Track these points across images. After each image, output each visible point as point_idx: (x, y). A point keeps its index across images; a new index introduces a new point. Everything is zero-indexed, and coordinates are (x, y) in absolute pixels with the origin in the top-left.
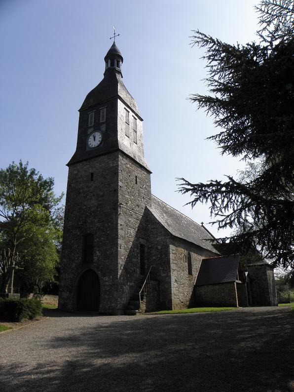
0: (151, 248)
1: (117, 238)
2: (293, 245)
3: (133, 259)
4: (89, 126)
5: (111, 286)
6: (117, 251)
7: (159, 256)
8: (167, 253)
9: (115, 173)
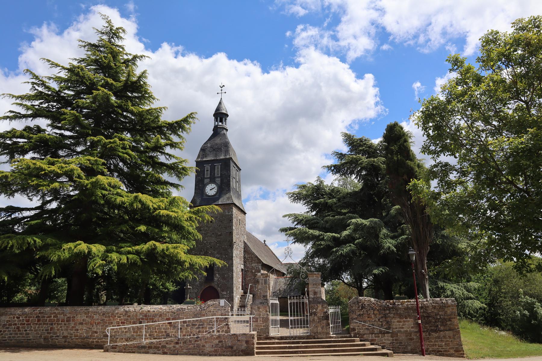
0: (247, 271)
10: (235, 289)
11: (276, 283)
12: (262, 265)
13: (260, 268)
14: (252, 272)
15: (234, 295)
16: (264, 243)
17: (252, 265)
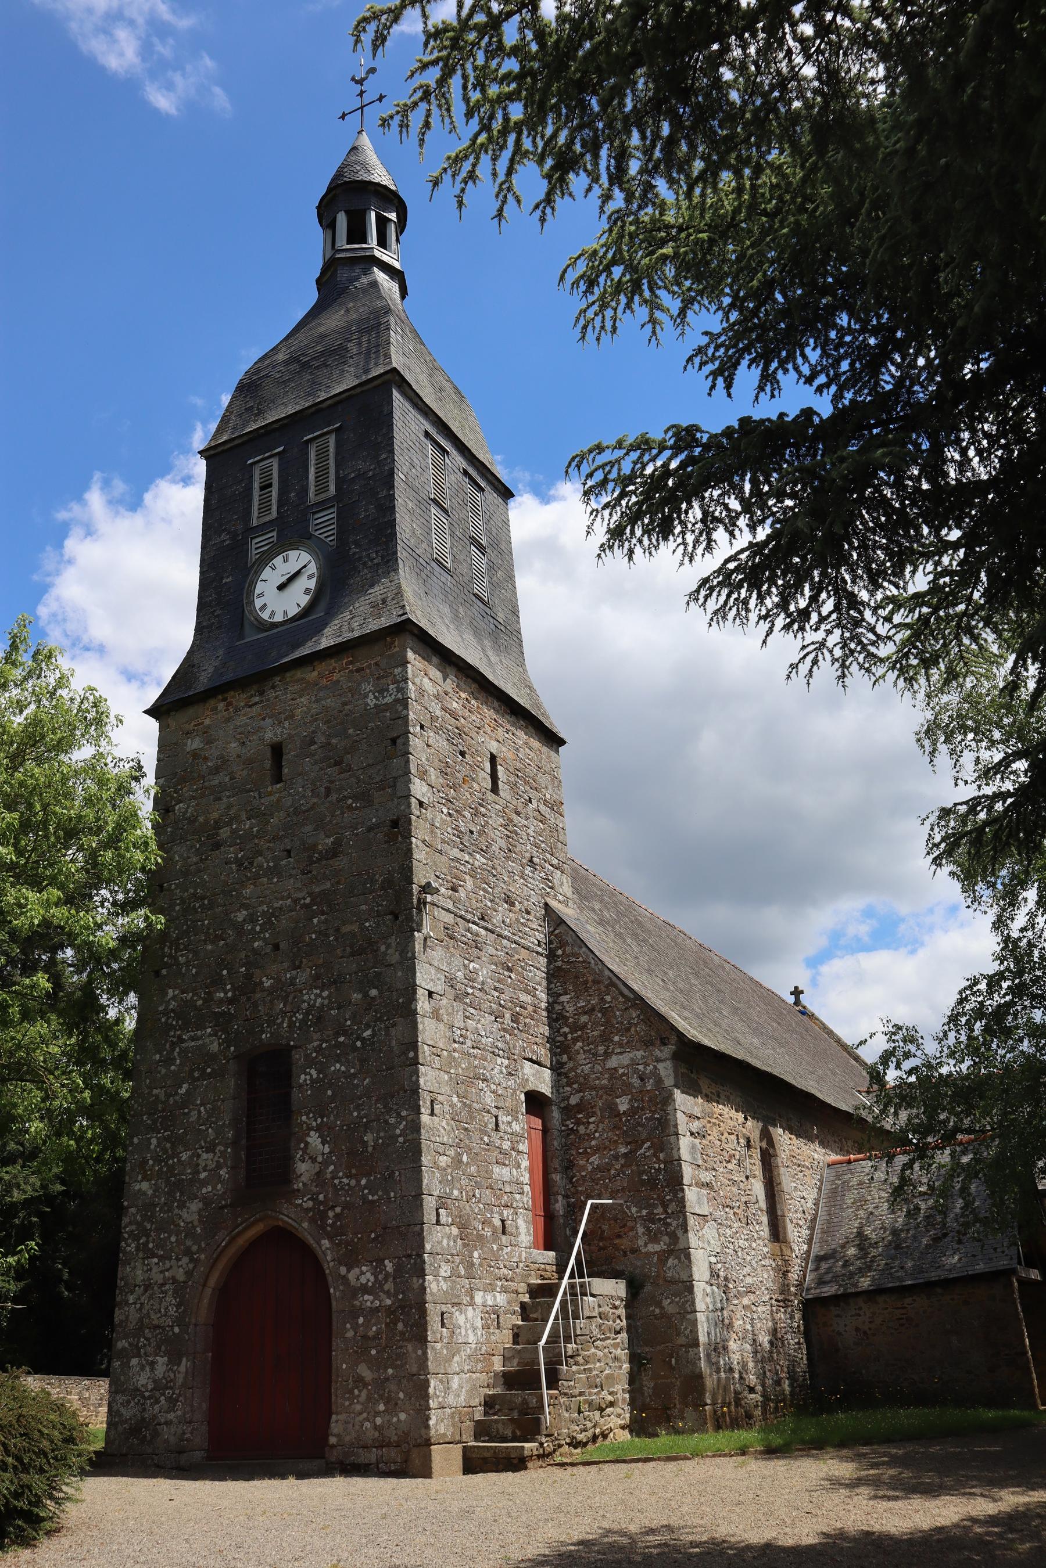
0: (580, 1107)
1: (415, 1062)
3: (497, 1169)
4: (255, 523)
5: (389, 1311)
6: (416, 1127)
7: (623, 1150)
9: (394, 741)
12: (676, 1057)
13: (669, 1081)
14: (612, 1110)
15: (436, 1285)
16: (797, 1002)
17: (613, 1062)
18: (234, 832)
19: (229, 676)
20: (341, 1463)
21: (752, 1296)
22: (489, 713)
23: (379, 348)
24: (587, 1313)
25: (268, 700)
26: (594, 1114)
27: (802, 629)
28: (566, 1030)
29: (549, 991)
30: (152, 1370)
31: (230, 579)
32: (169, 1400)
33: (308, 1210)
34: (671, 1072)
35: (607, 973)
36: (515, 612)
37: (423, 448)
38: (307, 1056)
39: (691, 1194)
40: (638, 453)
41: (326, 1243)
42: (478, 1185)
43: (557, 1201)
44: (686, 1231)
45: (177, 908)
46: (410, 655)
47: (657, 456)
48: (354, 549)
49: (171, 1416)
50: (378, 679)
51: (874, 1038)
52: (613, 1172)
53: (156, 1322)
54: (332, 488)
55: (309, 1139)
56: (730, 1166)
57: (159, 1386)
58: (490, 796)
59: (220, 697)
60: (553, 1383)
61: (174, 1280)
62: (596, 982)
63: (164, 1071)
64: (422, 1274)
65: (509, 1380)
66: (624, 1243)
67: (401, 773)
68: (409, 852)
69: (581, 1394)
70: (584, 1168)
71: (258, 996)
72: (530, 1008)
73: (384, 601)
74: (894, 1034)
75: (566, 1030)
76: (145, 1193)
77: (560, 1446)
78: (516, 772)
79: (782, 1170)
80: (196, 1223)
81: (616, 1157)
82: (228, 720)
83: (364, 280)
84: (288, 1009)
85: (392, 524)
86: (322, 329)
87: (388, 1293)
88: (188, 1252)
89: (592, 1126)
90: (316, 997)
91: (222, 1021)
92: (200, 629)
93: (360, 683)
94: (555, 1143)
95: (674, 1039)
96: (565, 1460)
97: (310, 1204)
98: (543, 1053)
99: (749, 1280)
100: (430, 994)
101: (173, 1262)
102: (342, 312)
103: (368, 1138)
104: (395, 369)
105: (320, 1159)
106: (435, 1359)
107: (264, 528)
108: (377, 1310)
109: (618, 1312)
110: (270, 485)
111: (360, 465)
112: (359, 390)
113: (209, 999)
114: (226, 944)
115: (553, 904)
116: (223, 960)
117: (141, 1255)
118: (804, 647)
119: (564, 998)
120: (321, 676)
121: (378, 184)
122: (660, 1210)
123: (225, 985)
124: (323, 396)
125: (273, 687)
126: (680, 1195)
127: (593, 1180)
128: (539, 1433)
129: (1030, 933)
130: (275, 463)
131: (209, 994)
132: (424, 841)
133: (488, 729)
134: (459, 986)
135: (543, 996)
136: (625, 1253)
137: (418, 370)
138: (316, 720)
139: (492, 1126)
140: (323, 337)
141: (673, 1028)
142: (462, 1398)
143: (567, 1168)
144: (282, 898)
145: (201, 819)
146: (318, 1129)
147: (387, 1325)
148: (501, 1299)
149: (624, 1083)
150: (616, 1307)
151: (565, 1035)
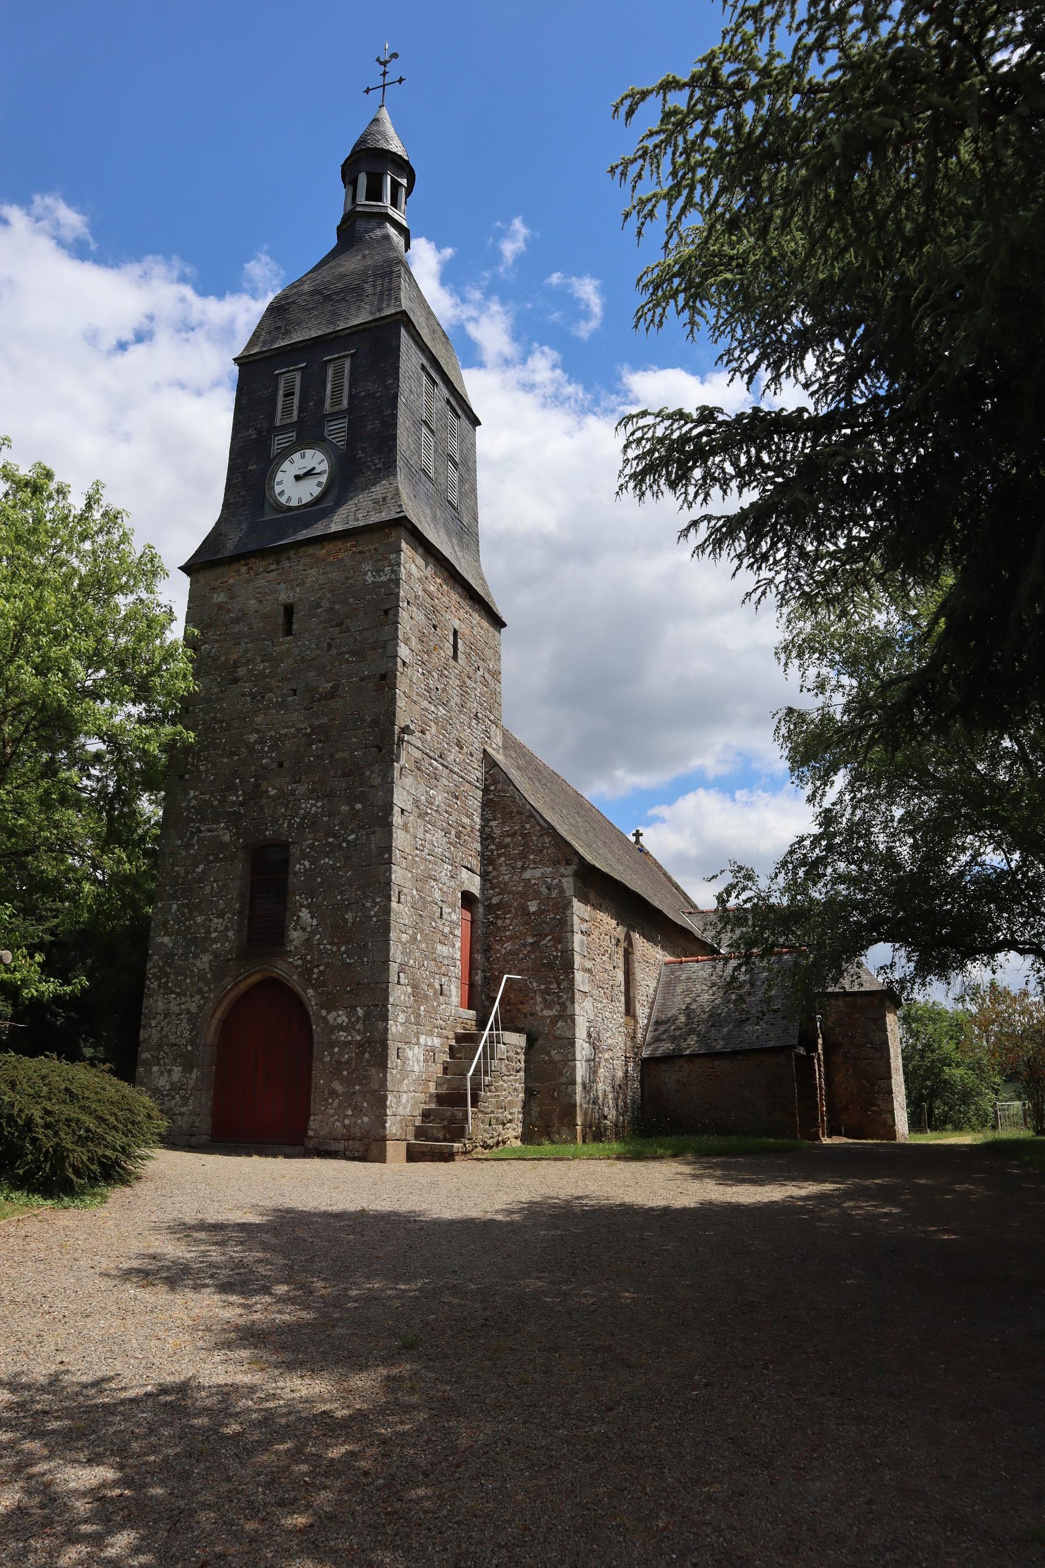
0: (499, 906)
1: (389, 862)
2: (10, 991)
3: (439, 947)
4: (278, 423)
5: (359, 1044)
6: (387, 911)
7: (530, 940)
8: (562, 929)
9: (386, 612)
10: (399, 994)
11: (668, 985)
12: (576, 874)
13: (569, 892)
14: (524, 910)
15: (395, 1028)
16: (637, 842)
17: (528, 874)
18: (250, 671)
19: (252, 546)
20: (317, 1149)
21: (611, 1053)
22: (455, 597)
23: (390, 292)
24: (500, 1056)
25: (283, 569)
26: (509, 912)
27: (759, 568)
28: (493, 847)
29: (483, 817)
30: (170, 1075)
31: (255, 467)
32: (183, 1098)
33: (297, 967)
34: (572, 885)
35: (528, 806)
36: (475, 518)
37: (419, 379)
38: (302, 850)
39: (579, 976)
40: (670, 421)
41: (311, 992)
42: (426, 958)
43: (477, 974)
44: (573, 1002)
45: (200, 727)
46: (404, 545)
47: (683, 426)
48: (360, 454)
49: (184, 1109)
50: (376, 561)
51: (723, 874)
52: (521, 956)
53: (173, 1041)
54: (345, 402)
55: (301, 914)
56: (604, 958)
57: (175, 1088)
58: (452, 662)
59: (243, 562)
60: (474, 1104)
61: (188, 1011)
62: (519, 813)
63: (184, 853)
64: (386, 1019)
65: (440, 1099)
66: (526, 1008)
67: (390, 637)
68: (393, 700)
69: (492, 1112)
70: (499, 951)
71: (264, 801)
72: (469, 829)
73: (384, 499)
74: (739, 872)
75: (493, 847)
76: (166, 945)
77: (476, 1147)
78: (470, 646)
79: (636, 964)
80: (207, 970)
81: (524, 945)
82: (249, 581)
83: (378, 233)
84: (288, 813)
85: (394, 438)
86: (342, 269)
87: (358, 1032)
88: (200, 991)
89: (507, 921)
90: (312, 806)
91: (233, 819)
92: (227, 505)
93: (361, 563)
94: (479, 931)
95: (576, 860)
96: (480, 1157)
97: (300, 962)
98: (475, 863)
99: (610, 1041)
100: (403, 811)
101: (188, 998)
102: (359, 257)
103: (349, 916)
104: (404, 312)
105: (309, 929)
106: (392, 1080)
107: (285, 428)
108: (349, 1043)
109: (519, 1057)
110: (293, 394)
111: (370, 386)
112: (373, 325)
113: (223, 801)
114: (240, 759)
115: (489, 750)
116: (236, 771)
117: (162, 991)
118: (758, 582)
119: (493, 823)
120: (329, 554)
121: (395, 154)
122: (554, 986)
123: (237, 791)
124: (342, 326)
125: (288, 559)
126: (571, 976)
127: (505, 961)
128: (463, 1137)
129: (838, 807)
130: (298, 377)
131: (224, 796)
132: (404, 693)
133: (454, 610)
134: (422, 807)
135: (478, 820)
136: (525, 1015)
137: (419, 314)
138: (323, 588)
139: (438, 914)
140: (343, 276)
141: (576, 853)
142: (408, 1109)
143: (486, 951)
144: (287, 727)
145: (223, 659)
146: (308, 907)
147: (356, 1054)
148: (437, 1042)
149: (535, 891)
150: (517, 1054)
151: (492, 851)
